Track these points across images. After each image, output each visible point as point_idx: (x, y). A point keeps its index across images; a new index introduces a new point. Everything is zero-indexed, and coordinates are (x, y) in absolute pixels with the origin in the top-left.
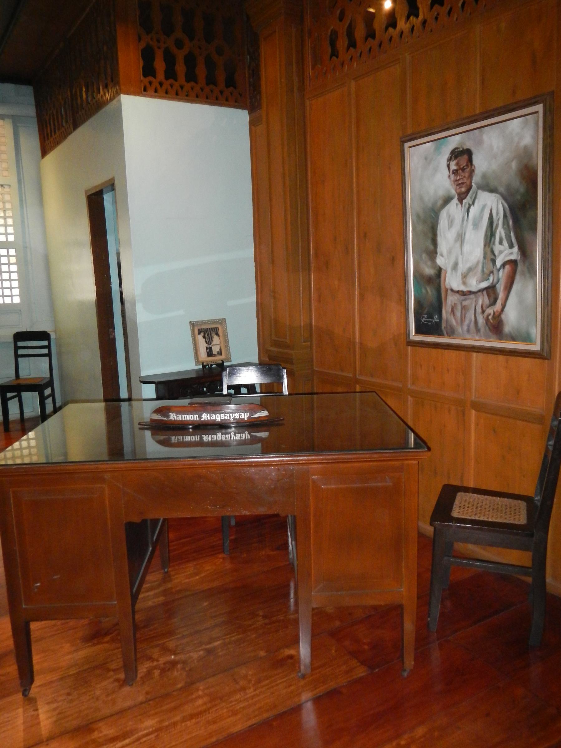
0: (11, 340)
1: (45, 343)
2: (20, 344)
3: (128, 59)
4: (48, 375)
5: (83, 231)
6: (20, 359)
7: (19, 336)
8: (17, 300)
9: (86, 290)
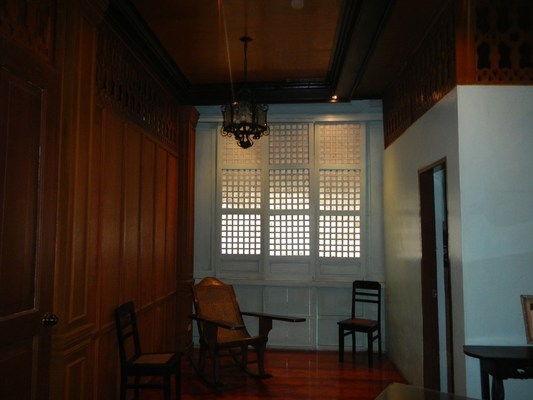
0: (351, 286)
1: (376, 292)
2: (358, 290)
3: (466, 54)
4: (376, 319)
5: (414, 203)
6: (356, 303)
7: (358, 284)
8: (358, 255)
9: (411, 248)
